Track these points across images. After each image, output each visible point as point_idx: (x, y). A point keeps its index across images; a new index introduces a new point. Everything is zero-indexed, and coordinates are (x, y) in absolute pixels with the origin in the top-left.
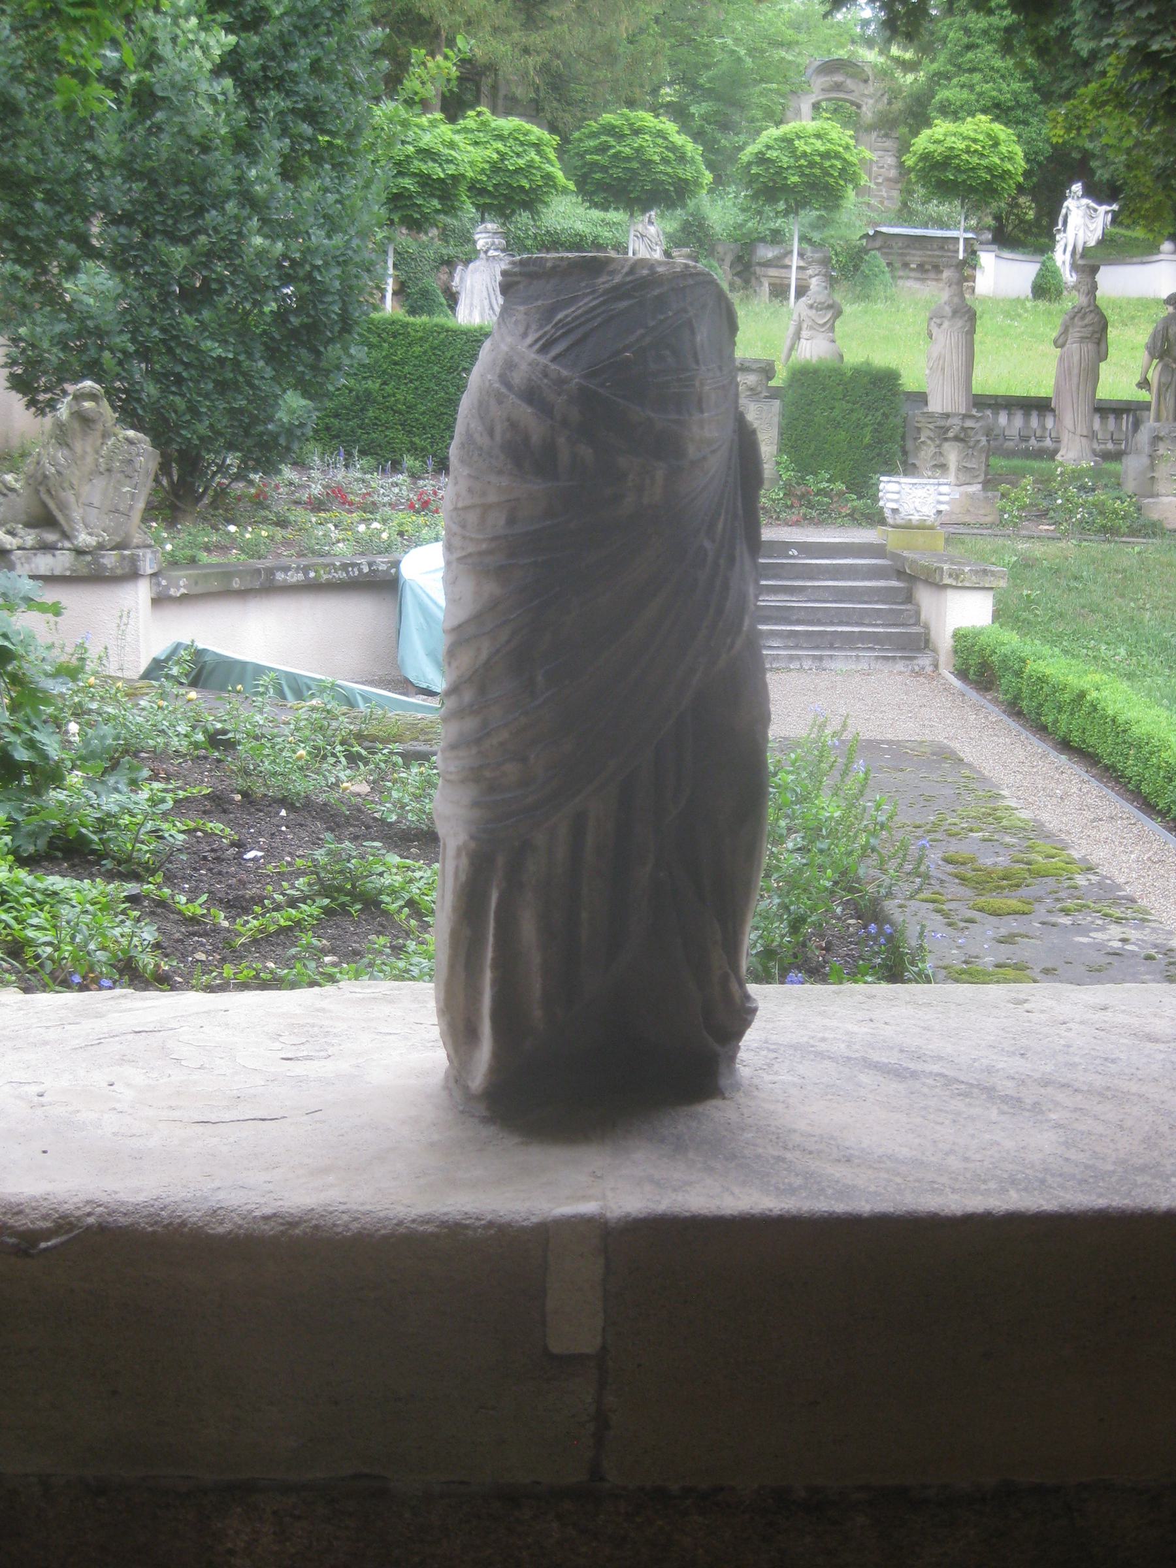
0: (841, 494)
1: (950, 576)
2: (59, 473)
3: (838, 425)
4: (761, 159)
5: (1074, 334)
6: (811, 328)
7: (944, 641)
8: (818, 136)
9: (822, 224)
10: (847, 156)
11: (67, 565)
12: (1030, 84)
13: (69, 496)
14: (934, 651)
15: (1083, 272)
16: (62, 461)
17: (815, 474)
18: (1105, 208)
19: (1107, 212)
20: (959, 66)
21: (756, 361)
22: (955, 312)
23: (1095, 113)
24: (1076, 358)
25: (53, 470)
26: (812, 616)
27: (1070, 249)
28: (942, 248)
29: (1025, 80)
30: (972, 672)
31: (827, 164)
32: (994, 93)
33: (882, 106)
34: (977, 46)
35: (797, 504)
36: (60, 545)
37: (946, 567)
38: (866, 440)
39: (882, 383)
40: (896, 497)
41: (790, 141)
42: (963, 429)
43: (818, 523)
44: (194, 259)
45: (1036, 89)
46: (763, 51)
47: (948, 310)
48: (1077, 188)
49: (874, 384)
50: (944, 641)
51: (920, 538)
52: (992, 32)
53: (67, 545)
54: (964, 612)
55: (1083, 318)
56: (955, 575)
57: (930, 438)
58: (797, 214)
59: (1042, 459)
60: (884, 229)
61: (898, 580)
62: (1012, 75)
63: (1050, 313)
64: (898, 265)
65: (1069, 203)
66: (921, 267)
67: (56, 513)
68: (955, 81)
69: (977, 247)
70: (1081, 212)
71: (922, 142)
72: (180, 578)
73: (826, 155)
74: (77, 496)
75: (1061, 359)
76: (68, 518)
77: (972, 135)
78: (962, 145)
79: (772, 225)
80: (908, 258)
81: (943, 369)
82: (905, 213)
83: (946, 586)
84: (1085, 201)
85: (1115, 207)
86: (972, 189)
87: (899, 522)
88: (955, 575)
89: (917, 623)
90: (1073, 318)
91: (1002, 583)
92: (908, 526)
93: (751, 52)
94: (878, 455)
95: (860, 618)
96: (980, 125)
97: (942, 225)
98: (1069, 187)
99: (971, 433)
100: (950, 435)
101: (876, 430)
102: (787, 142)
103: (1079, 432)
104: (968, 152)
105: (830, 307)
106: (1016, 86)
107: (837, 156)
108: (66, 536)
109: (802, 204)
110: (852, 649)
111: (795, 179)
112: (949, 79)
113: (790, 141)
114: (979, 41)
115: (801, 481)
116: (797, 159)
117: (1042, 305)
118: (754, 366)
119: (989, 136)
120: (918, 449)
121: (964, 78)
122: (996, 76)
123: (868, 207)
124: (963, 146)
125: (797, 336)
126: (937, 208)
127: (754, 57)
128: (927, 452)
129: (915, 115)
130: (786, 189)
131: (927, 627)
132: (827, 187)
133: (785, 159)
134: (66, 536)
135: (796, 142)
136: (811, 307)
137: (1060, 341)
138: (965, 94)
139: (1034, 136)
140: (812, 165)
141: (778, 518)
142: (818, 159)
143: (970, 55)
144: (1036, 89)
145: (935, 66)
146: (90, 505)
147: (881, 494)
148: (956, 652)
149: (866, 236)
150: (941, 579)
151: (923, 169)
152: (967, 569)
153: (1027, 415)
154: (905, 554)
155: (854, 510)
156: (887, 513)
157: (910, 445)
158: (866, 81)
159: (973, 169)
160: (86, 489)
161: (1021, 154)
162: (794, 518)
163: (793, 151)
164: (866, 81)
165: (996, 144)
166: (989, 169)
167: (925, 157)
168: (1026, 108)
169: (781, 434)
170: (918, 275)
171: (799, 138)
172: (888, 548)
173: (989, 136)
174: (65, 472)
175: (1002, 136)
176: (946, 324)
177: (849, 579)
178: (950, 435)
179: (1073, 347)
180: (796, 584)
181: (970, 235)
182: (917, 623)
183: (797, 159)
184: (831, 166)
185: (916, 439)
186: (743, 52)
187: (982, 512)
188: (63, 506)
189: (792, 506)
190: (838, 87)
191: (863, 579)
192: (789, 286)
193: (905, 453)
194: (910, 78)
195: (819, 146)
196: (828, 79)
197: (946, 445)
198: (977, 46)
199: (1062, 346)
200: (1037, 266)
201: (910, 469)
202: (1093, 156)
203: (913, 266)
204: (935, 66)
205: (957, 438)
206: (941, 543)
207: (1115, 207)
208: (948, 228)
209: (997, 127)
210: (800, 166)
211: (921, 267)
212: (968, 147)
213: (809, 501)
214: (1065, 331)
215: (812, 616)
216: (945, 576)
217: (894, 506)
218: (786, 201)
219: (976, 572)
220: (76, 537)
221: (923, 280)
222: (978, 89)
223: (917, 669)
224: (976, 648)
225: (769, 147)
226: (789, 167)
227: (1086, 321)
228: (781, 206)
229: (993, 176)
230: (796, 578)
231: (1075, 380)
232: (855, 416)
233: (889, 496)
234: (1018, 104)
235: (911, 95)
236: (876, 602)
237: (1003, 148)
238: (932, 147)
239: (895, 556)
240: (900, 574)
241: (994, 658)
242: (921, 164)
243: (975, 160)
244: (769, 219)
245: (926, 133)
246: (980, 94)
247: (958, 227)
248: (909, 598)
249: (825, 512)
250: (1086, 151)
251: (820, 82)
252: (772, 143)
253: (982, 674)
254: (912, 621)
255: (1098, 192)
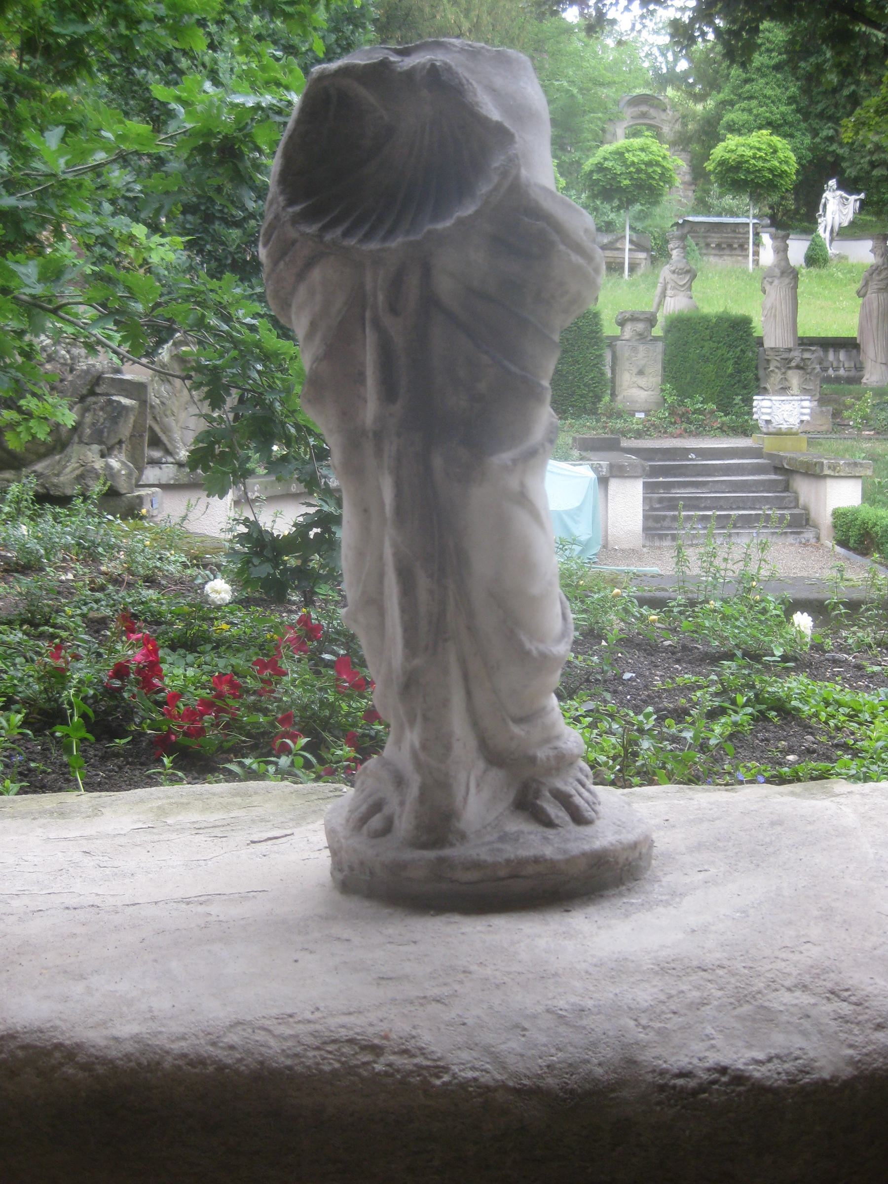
0: (712, 412)
1: (829, 468)
2: (163, 403)
3: (707, 360)
4: (600, 168)
5: (873, 286)
6: (673, 288)
7: (825, 520)
8: (642, 150)
9: (641, 217)
10: (665, 164)
11: (171, 475)
12: (794, 107)
13: (170, 421)
14: (815, 526)
15: (878, 239)
16: (165, 394)
17: (691, 397)
18: (853, 198)
19: (856, 201)
20: (740, 96)
21: (643, 313)
22: (783, 273)
23: (877, 119)
24: (875, 305)
25: (158, 401)
26: (716, 504)
27: (829, 229)
28: (734, 231)
29: (789, 104)
30: (852, 541)
31: (650, 170)
32: (768, 115)
33: (678, 127)
34: (753, 80)
35: (678, 421)
36: (164, 460)
37: (825, 462)
38: (729, 371)
39: (738, 328)
40: (769, 411)
41: (621, 154)
42: (802, 359)
43: (697, 435)
44: (245, 239)
45: (798, 111)
46: (589, 90)
47: (777, 272)
48: (833, 183)
49: (733, 327)
50: (825, 520)
51: (788, 442)
52: (764, 69)
53: (170, 459)
54: (842, 495)
55: (879, 274)
56: (833, 467)
57: (777, 367)
58: (627, 208)
59: (840, 383)
60: (690, 219)
61: (776, 474)
62: (780, 100)
63: (820, 277)
64: (703, 245)
65: (827, 195)
66: (719, 246)
67: (161, 434)
68: (737, 107)
69: (759, 230)
70: (836, 201)
71: (719, 152)
72: (254, 484)
73: (649, 164)
74: (177, 421)
75: (863, 304)
76: (171, 439)
77: (757, 145)
78: (750, 153)
79: (606, 219)
80: (709, 240)
81: (775, 316)
82: (702, 205)
83: (826, 476)
84: (839, 193)
85: (862, 196)
86: (758, 186)
87: (772, 430)
88: (833, 467)
89: (797, 506)
90: (871, 274)
91: (869, 473)
92: (779, 433)
93: (581, 90)
94: (739, 381)
95: (753, 503)
96: (762, 138)
97: (733, 214)
98: (827, 183)
99: (809, 363)
100: (793, 364)
101: (736, 363)
102: (620, 154)
103: (879, 360)
104: (754, 158)
105: (688, 272)
106: (783, 108)
107: (658, 164)
108: (168, 452)
109: (631, 202)
110: (750, 528)
111: (627, 182)
112: (733, 106)
113: (621, 154)
114: (754, 76)
115: (681, 403)
116: (628, 167)
117: (814, 271)
118: (642, 317)
119: (770, 145)
120: (768, 376)
121: (744, 104)
122: (768, 101)
123: (677, 202)
124: (751, 154)
125: (664, 295)
126: (728, 200)
127: (583, 94)
128: (775, 379)
129: (706, 133)
130: (620, 190)
131: (806, 508)
132: (651, 188)
133: (619, 168)
134: (168, 452)
135: (626, 155)
136: (674, 272)
137: (862, 292)
138: (745, 116)
139: (798, 145)
140: (639, 171)
141: (665, 432)
142: (643, 167)
143: (748, 87)
144: (798, 111)
145: (721, 96)
146: (187, 428)
147: (754, 410)
148: (835, 527)
149: (677, 224)
150: (822, 470)
151: (721, 172)
152: (842, 462)
153: (826, 351)
154: (781, 454)
155: (723, 424)
156: (761, 424)
157: (761, 373)
158: (664, 110)
159: (759, 171)
160: (183, 416)
161: (794, 158)
162: (678, 432)
163: (624, 162)
164: (664, 110)
165: (775, 152)
166: (771, 170)
167: (722, 163)
168: (791, 125)
169: (664, 368)
170: (717, 252)
171: (628, 151)
172: (765, 450)
173: (770, 145)
174: (167, 402)
175: (779, 146)
176: (776, 282)
177: (739, 475)
178: (793, 364)
179: (872, 296)
180: (700, 479)
181: (756, 221)
182: (797, 506)
183: (628, 167)
184: (654, 172)
185: (765, 369)
186: (575, 91)
187: (819, 422)
188: (166, 430)
189: (675, 423)
190: (644, 115)
191: (749, 474)
192: (623, 263)
193: (757, 379)
194: (699, 107)
195: (643, 156)
196: (636, 109)
197: (790, 372)
198: (753, 80)
199: (864, 296)
200: (807, 244)
201: (764, 391)
202: (843, 159)
203: (713, 245)
204: (721, 96)
205: (798, 367)
206: (804, 445)
207: (862, 196)
208: (738, 216)
209: (776, 139)
210: (630, 173)
211: (719, 246)
212: (755, 154)
213: (688, 418)
214: (866, 285)
215: (716, 504)
216: (825, 468)
217: (768, 418)
218: (620, 199)
219: (849, 465)
220: (178, 454)
221: (721, 256)
222: (755, 112)
223: (803, 541)
224: (858, 522)
225: (605, 159)
226: (621, 174)
227: (882, 276)
228: (616, 203)
229: (774, 175)
230: (698, 475)
231: (875, 321)
232: (720, 352)
233: (763, 410)
234: (786, 123)
235: (703, 118)
236: (762, 492)
237: (780, 155)
238: (727, 155)
239: (770, 456)
240: (778, 469)
241: (877, 528)
242: (719, 169)
243: (760, 164)
244: (604, 214)
245: (722, 144)
246: (757, 116)
247: (747, 214)
248: (787, 488)
249: (701, 426)
250: (838, 155)
251: (629, 112)
252: (608, 156)
253: (862, 542)
254: (792, 505)
255: (848, 186)
